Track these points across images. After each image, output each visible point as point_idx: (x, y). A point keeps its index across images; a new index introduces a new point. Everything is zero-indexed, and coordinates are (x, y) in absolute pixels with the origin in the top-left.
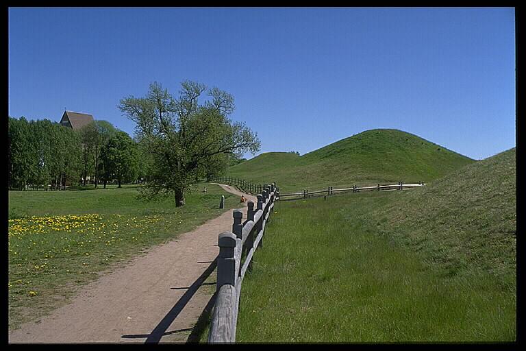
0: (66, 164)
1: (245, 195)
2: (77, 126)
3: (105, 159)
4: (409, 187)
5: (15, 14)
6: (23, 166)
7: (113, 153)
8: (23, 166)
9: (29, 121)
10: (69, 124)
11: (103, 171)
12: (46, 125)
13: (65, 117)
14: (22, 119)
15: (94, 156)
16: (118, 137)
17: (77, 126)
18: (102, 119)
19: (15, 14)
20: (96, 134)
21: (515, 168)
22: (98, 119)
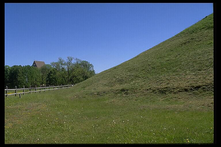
0: (36, 80)
1: (12, 94)
2: (39, 67)
3: (49, 78)
4: (67, 86)
5: (8, 7)
6: (21, 82)
7: (51, 76)
8: (21, 82)
9: (22, 66)
10: (36, 66)
11: (49, 82)
12: (28, 67)
13: (34, 63)
14: (20, 66)
15: (45, 78)
16: (53, 70)
17: (39, 67)
18: (47, 64)
19: (8, 7)
20: (54, 72)
21: (213, 42)
22: (46, 64)
